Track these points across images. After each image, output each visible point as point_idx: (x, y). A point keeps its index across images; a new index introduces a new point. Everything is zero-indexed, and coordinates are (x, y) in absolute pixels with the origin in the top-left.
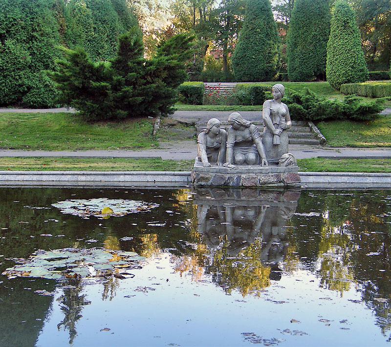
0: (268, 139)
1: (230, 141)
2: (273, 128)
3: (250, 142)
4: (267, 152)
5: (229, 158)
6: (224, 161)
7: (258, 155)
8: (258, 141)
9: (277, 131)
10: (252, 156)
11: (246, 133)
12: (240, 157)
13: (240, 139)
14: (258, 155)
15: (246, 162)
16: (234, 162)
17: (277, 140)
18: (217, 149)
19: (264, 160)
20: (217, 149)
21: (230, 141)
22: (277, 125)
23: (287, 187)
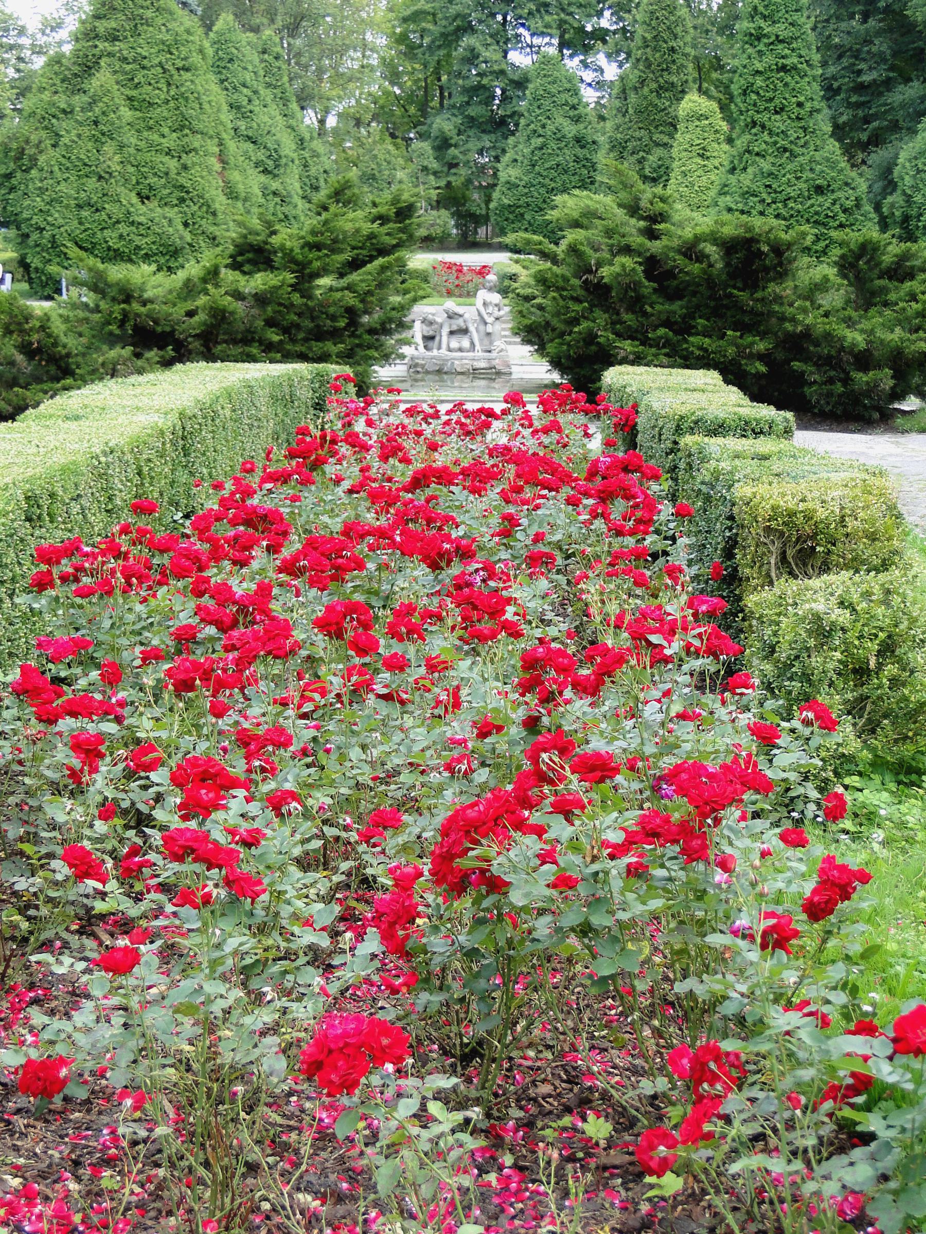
0: (482, 327)
1: (445, 331)
2: (486, 317)
3: (465, 331)
4: (481, 340)
5: (444, 345)
6: (439, 348)
7: (472, 344)
8: (472, 329)
9: (490, 320)
10: (466, 343)
11: (460, 322)
12: (454, 344)
13: (455, 328)
14: (472, 344)
15: (461, 350)
16: (450, 350)
17: (489, 329)
18: (432, 338)
19: (478, 347)
20: (432, 338)
21: (445, 331)
22: (490, 314)
23: (499, 373)
